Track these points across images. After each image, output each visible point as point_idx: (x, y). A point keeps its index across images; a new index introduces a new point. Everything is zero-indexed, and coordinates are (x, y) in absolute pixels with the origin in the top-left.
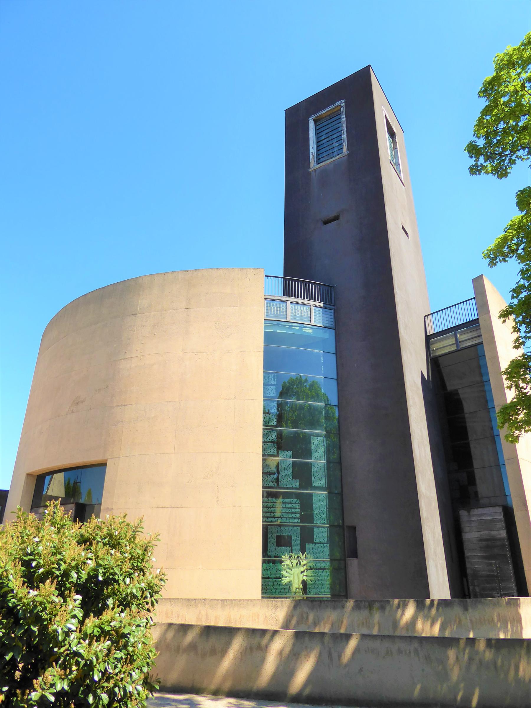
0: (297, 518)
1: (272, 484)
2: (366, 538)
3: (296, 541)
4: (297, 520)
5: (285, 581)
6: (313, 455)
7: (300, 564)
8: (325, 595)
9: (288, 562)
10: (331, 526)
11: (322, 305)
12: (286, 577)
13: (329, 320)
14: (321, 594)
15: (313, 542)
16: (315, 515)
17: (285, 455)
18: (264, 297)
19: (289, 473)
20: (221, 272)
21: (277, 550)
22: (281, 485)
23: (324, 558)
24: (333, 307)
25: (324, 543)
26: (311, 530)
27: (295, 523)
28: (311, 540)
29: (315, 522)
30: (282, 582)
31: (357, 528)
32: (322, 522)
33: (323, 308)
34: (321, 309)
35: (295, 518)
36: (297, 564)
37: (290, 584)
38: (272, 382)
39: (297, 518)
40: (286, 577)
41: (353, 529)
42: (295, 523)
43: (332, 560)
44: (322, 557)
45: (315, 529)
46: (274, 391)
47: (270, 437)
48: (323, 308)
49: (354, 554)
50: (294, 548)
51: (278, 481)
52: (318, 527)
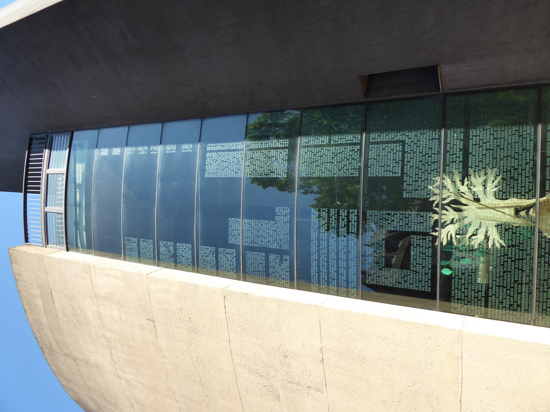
0: (348, 216)
1: (286, 264)
2: (386, 57)
3: (398, 221)
4: (353, 218)
5: (496, 239)
6: (233, 175)
7: (456, 202)
8: (534, 175)
9: (452, 229)
10: (365, 129)
11: (47, 151)
12: (487, 238)
13: (60, 139)
14: (535, 161)
15: (401, 180)
16: (342, 174)
17: (235, 232)
18: (44, 248)
19: (265, 227)
20: (26, 307)
21: (419, 268)
22: (286, 247)
23: (439, 152)
24: (50, 134)
25: (404, 152)
26: (374, 183)
27: (358, 221)
28: (395, 184)
29: (356, 174)
30: (498, 245)
31: (367, 73)
32: (356, 156)
33: (51, 149)
34: (52, 152)
35: (349, 221)
36: (456, 210)
37: (504, 229)
38: (135, 245)
39: (348, 216)
40: (487, 238)
41: (372, 82)
42: (358, 221)
43: (444, 124)
44: (434, 158)
45: (374, 172)
46: (145, 243)
47: (208, 259)
48: (51, 149)
49: (430, 73)
50: (414, 228)
51: (280, 252)
52: (366, 166)
